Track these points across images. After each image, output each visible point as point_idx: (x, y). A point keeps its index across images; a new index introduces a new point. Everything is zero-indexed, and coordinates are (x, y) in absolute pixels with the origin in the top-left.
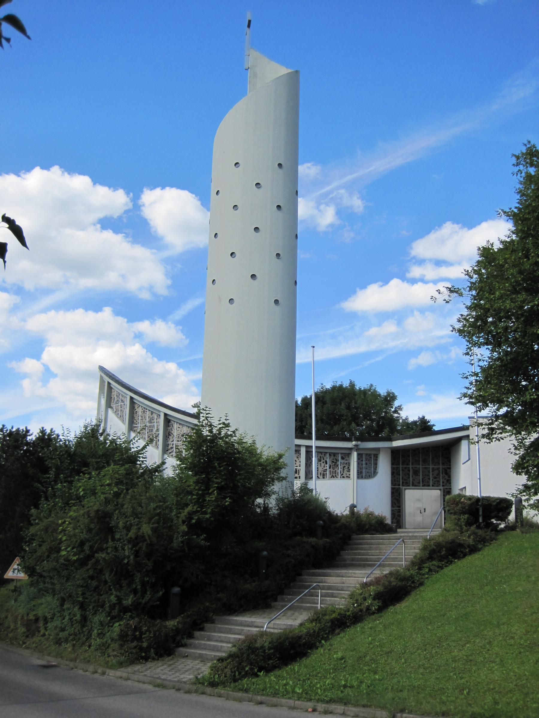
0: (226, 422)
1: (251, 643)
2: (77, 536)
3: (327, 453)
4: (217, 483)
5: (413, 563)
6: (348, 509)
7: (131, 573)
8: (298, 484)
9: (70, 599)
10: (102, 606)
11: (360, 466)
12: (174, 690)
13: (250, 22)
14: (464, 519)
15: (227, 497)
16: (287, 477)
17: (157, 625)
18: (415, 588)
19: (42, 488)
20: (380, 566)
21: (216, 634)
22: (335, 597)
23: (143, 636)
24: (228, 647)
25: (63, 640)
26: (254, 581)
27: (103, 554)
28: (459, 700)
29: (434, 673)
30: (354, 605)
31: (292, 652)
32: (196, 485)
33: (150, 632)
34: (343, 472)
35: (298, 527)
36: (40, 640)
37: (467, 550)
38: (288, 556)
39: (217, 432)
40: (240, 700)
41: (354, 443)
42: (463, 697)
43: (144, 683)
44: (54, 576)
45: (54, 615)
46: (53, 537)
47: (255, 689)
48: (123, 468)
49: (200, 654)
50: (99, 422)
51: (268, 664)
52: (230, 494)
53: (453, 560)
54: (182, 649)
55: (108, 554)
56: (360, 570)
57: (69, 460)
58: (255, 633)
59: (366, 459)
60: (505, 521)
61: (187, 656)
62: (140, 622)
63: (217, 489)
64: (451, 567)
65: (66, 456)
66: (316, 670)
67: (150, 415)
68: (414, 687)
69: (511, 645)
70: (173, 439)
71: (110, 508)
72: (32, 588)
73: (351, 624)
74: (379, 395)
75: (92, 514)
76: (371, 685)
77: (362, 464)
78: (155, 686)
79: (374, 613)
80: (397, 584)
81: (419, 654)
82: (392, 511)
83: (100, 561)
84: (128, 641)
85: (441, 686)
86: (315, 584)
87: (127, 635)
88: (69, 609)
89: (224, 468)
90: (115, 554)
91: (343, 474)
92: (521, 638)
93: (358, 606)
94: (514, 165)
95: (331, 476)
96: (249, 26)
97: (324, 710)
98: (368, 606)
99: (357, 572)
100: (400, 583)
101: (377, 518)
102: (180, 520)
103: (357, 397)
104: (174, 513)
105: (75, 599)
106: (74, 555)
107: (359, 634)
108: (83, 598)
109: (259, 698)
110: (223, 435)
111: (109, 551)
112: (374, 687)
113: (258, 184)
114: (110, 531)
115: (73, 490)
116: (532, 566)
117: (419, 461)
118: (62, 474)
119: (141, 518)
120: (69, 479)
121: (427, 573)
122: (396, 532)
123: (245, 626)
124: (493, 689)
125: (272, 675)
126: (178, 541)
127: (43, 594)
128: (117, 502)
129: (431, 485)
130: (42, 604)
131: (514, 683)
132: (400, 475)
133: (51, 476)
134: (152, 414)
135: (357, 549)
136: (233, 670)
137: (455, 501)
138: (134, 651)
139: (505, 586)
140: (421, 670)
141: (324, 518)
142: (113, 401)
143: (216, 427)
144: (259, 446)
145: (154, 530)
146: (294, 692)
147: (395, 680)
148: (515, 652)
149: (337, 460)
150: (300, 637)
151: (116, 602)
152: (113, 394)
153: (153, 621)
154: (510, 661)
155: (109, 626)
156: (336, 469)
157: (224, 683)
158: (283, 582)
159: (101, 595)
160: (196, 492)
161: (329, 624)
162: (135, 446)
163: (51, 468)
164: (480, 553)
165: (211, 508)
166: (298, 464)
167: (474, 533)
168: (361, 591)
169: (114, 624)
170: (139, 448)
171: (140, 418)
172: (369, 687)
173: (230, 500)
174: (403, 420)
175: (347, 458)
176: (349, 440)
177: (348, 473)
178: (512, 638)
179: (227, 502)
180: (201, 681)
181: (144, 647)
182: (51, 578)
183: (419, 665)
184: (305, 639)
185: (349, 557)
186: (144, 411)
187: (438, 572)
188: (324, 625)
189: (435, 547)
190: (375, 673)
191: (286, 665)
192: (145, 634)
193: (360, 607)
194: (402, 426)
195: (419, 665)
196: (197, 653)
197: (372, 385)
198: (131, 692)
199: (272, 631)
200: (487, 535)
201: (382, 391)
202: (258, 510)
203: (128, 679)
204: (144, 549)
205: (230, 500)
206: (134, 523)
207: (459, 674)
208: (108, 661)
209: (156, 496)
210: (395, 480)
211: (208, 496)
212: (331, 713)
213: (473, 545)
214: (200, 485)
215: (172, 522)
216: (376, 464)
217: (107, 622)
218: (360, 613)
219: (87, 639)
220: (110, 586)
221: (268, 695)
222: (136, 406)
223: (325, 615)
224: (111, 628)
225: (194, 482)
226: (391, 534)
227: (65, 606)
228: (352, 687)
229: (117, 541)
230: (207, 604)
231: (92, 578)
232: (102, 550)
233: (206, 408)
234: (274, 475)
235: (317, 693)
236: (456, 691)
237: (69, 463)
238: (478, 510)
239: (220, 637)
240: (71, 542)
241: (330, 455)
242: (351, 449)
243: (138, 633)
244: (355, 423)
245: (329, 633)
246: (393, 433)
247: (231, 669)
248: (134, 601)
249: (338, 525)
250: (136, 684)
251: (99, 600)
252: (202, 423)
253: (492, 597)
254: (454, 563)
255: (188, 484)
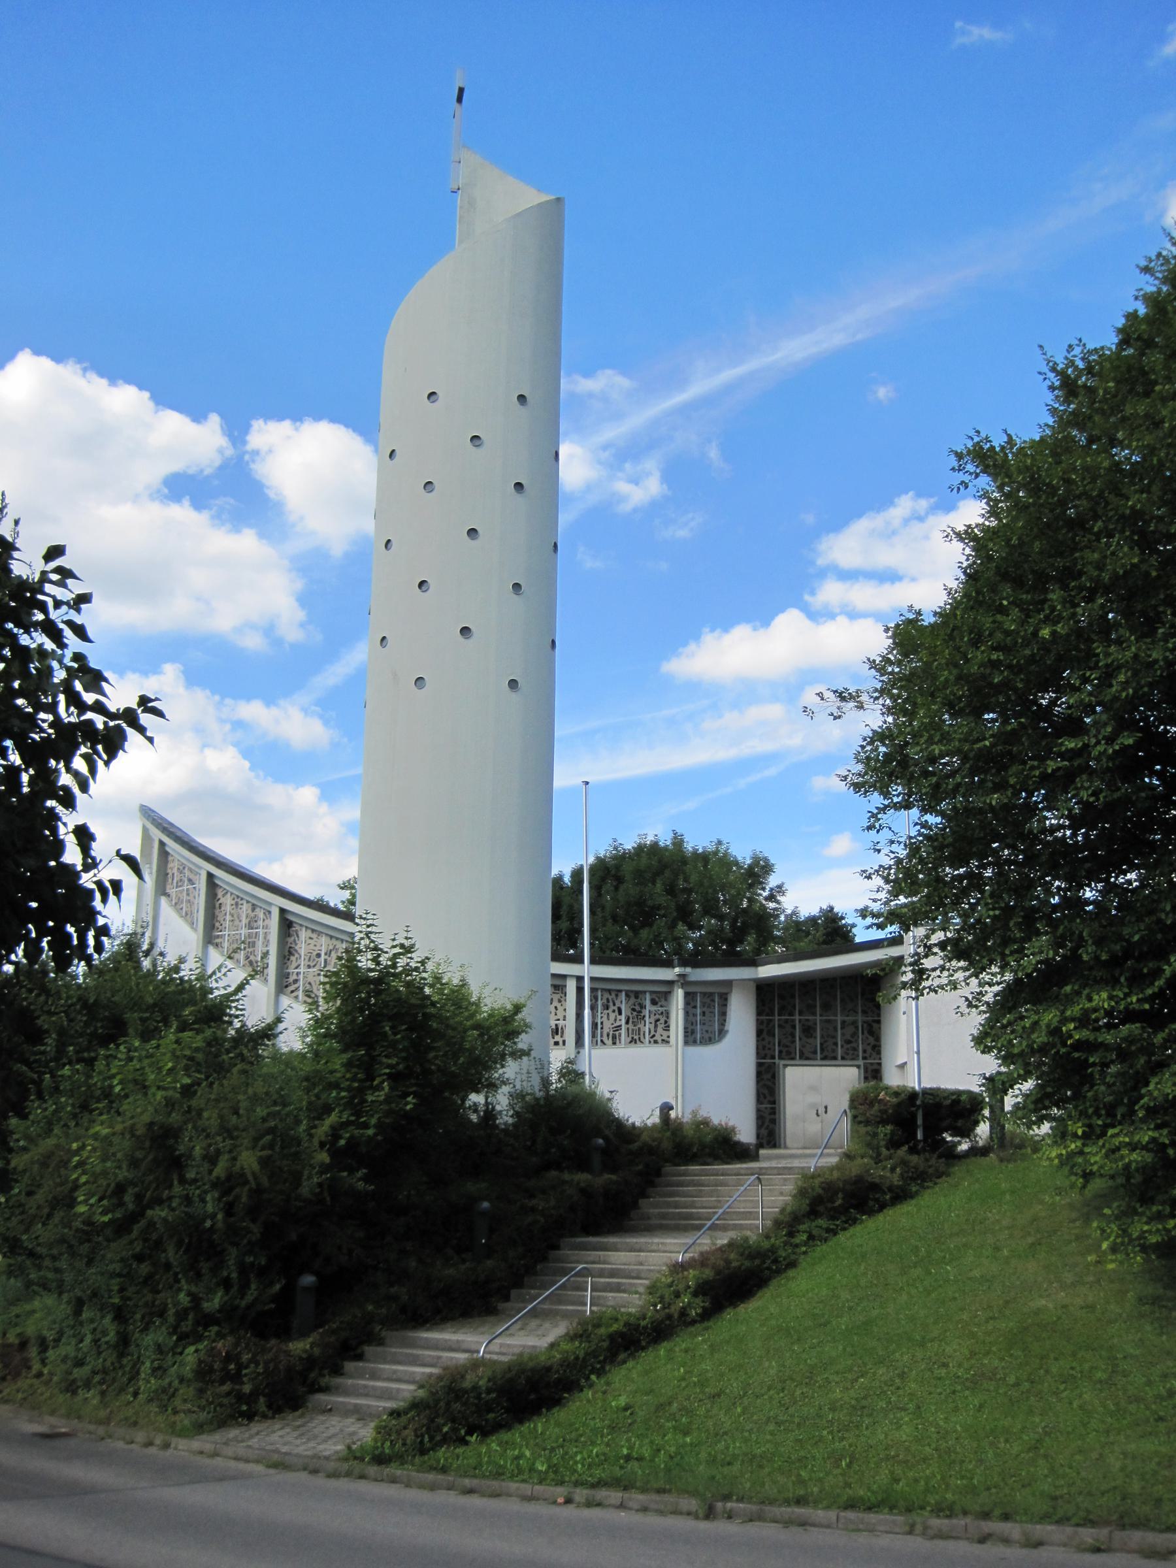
0: (407, 943)
1: (453, 1381)
2: (108, 1174)
3: (620, 991)
4: (389, 1066)
5: (777, 1223)
6: (657, 1112)
7: (219, 1249)
8: (557, 1058)
9: (95, 1300)
10: (162, 1314)
11: (691, 1018)
12: (306, 1472)
13: (461, 91)
14: (886, 1135)
15: (407, 1095)
16: (530, 1050)
17: (272, 1348)
18: (779, 1272)
19: (31, 1074)
20: (714, 1227)
21: (387, 1367)
22: (624, 1291)
23: (244, 1372)
24: (409, 1391)
25: (79, 1383)
26: (464, 1261)
27: (162, 1210)
28: (831, 1477)
29: (792, 1431)
30: (655, 1306)
31: (532, 1397)
32: (348, 1071)
33: (257, 1364)
34: (656, 1031)
35: (553, 1150)
36: (31, 1386)
37: (888, 1197)
38: (533, 1210)
39: (389, 963)
40: (433, 1487)
41: (677, 970)
42: (838, 1471)
43: (247, 1461)
44: (61, 1254)
45: (61, 1333)
46: (60, 1176)
47: (459, 1467)
48: (199, 1037)
49: (356, 1405)
50: (142, 927)
51: (487, 1420)
52: (414, 1089)
53: (858, 1216)
54: (322, 1397)
55: (173, 1210)
56: (675, 1238)
57: (85, 1015)
58: (462, 1362)
59: (703, 1005)
60: (968, 1136)
61: (330, 1410)
62: (237, 1345)
63: (388, 1079)
64: (852, 1230)
65: (78, 1007)
66: (577, 1430)
67: (250, 911)
68: (754, 1456)
69: (940, 1379)
70: (298, 962)
71: (175, 1118)
72: (12, 1280)
73: (649, 1343)
74: (736, 863)
75: (140, 1132)
76: (677, 1454)
77: (695, 1015)
78: (269, 1466)
79: (693, 1322)
80: (742, 1264)
81: (771, 1398)
82: (758, 1111)
83: (155, 1223)
84: (212, 1383)
85: (802, 1453)
86: (581, 1266)
87: (211, 1370)
88: (92, 1321)
89: (403, 1038)
90: (186, 1209)
91: (654, 1036)
92: (960, 1365)
93: (663, 1308)
94: (953, 469)
95: (630, 1039)
96: (460, 99)
97: (587, 1499)
98: (683, 1308)
99: (668, 1241)
100: (747, 1264)
101: (716, 1129)
102: (316, 1142)
103: (688, 868)
104: (303, 1127)
105: (104, 1300)
106: (104, 1213)
107: (663, 1361)
108: (122, 1298)
109: (467, 1482)
110: (400, 969)
111: (174, 1205)
112: (682, 1458)
113: (475, 438)
114: (175, 1164)
115: (95, 1080)
116: (1008, 1228)
117: (816, 1006)
118: (71, 1045)
119: (237, 1137)
120: (86, 1055)
121: (806, 1244)
122: (756, 1158)
123: (444, 1349)
124: (893, 1457)
125: (493, 1441)
126: (309, 1184)
127: (35, 1293)
128: (189, 1107)
129: (839, 1058)
130: (34, 1311)
131: (934, 1446)
132: (774, 1035)
133: (49, 1049)
134: (253, 910)
135: (672, 1195)
136: (419, 1433)
137: (866, 1099)
138: (225, 1401)
139: (948, 1268)
140: (771, 1427)
141: (607, 1132)
142: (170, 880)
143: (386, 952)
144: (474, 991)
145: (264, 1162)
146: (532, 1469)
147: (721, 1446)
148: (945, 1390)
149: (642, 1007)
150: (548, 1369)
151: (189, 1305)
152: (170, 865)
153: (262, 1342)
154: (933, 1408)
155: (174, 1354)
156: (641, 1026)
157: (401, 1457)
158: (522, 1262)
159: (158, 1292)
160: (348, 1083)
161: (605, 1344)
162: (221, 984)
163: (47, 1031)
164: (913, 1202)
165: (377, 1116)
166: (560, 1014)
167: (904, 1163)
168: (670, 1280)
169: (184, 1348)
170: (230, 990)
171: (228, 917)
172: (671, 1457)
173: (414, 1101)
174: (786, 916)
175: (663, 1002)
176: (668, 964)
177: (665, 1034)
178: (945, 1365)
179: (407, 1104)
180: (358, 1454)
181: (245, 1394)
182: (54, 1258)
183: (769, 1418)
184: (557, 1372)
185: (657, 1211)
186: (237, 904)
187: (826, 1240)
188: (597, 1345)
189: (821, 1191)
190: (686, 1434)
191: (521, 1422)
192: (246, 1368)
193: (667, 1311)
194: (786, 929)
195: (769, 1418)
196: (349, 1403)
197: (720, 843)
198: (222, 1477)
199: (495, 1357)
200: (930, 1167)
201: (742, 853)
202: (474, 1117)
203: (215, 1454)
204: (244, 1199)
205: (414, 1101)
206: (224, 1147)
207: (839, 1432)
208: (175, 1423)
209: (267, 1094)
210: (764, 1047)
211: (370, 1092)
212: (599, 1505)
213: (898, 1187)
214: (354, 1070)
215: (299, 1144)
216: (724, 1014)
217: (172, 1344)
218: (668, 1322)
219: (130, 1380)
220: (176, 1274)
221: (484, 1477)
222: (220, 893)
223: (597, 1326)
224: (180, 1358)
225: (343, 1065)
226: (745, 1162)
227: (84, 1315)
228: (640, 1459)
229: (190, 1185)
230: (370, 1308)
231: (139, 1258)
232: (158, 1201)
233: (367, 914)
234: (506, 1046)
235: (575, 1471)
236: (828, 1462)
237: (86, 1022)
238: (914, 1117)
239: (395, 1372)
240: (98, 1187)
241: (627, 996)
242: (670, 983)
243: (232, 1366)
244: (685, 922)
245: (604, 1361)
246: (765, 944)
247: (416, 1430)
248: (226, 1303)
249: (635, 1146)
250: (232, 1464)
251: (153, 1302)
252: (359, 943)
253: (921, 1289)
254: (860, 1223)
255: (330, 1068)
